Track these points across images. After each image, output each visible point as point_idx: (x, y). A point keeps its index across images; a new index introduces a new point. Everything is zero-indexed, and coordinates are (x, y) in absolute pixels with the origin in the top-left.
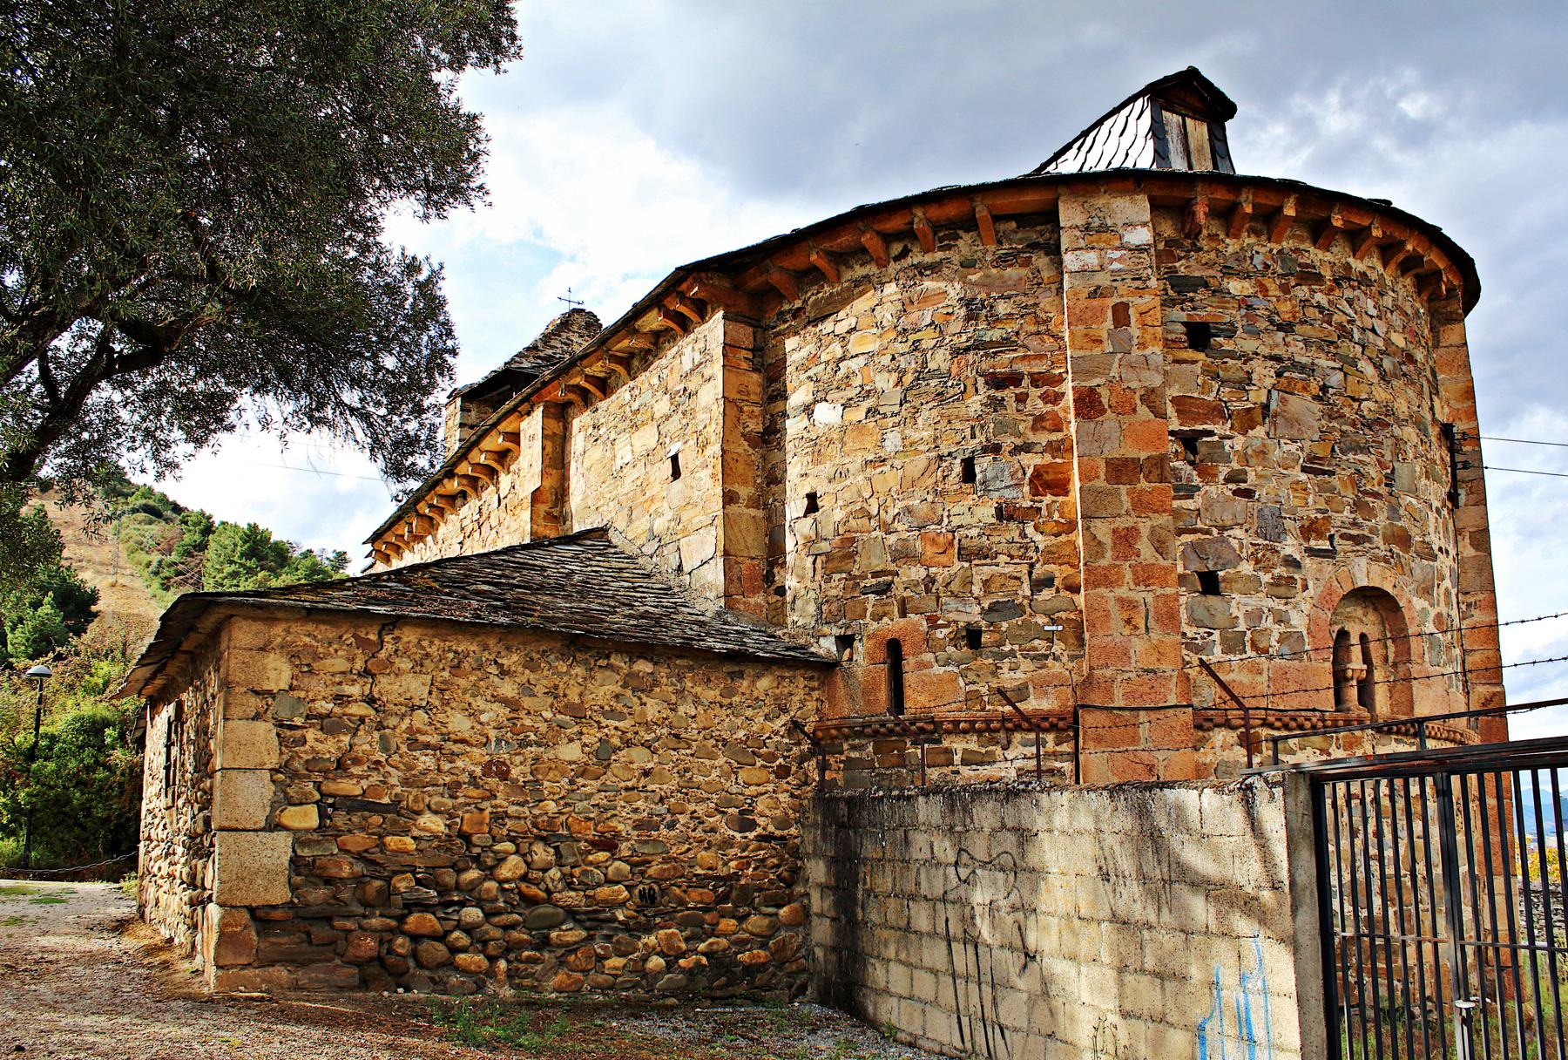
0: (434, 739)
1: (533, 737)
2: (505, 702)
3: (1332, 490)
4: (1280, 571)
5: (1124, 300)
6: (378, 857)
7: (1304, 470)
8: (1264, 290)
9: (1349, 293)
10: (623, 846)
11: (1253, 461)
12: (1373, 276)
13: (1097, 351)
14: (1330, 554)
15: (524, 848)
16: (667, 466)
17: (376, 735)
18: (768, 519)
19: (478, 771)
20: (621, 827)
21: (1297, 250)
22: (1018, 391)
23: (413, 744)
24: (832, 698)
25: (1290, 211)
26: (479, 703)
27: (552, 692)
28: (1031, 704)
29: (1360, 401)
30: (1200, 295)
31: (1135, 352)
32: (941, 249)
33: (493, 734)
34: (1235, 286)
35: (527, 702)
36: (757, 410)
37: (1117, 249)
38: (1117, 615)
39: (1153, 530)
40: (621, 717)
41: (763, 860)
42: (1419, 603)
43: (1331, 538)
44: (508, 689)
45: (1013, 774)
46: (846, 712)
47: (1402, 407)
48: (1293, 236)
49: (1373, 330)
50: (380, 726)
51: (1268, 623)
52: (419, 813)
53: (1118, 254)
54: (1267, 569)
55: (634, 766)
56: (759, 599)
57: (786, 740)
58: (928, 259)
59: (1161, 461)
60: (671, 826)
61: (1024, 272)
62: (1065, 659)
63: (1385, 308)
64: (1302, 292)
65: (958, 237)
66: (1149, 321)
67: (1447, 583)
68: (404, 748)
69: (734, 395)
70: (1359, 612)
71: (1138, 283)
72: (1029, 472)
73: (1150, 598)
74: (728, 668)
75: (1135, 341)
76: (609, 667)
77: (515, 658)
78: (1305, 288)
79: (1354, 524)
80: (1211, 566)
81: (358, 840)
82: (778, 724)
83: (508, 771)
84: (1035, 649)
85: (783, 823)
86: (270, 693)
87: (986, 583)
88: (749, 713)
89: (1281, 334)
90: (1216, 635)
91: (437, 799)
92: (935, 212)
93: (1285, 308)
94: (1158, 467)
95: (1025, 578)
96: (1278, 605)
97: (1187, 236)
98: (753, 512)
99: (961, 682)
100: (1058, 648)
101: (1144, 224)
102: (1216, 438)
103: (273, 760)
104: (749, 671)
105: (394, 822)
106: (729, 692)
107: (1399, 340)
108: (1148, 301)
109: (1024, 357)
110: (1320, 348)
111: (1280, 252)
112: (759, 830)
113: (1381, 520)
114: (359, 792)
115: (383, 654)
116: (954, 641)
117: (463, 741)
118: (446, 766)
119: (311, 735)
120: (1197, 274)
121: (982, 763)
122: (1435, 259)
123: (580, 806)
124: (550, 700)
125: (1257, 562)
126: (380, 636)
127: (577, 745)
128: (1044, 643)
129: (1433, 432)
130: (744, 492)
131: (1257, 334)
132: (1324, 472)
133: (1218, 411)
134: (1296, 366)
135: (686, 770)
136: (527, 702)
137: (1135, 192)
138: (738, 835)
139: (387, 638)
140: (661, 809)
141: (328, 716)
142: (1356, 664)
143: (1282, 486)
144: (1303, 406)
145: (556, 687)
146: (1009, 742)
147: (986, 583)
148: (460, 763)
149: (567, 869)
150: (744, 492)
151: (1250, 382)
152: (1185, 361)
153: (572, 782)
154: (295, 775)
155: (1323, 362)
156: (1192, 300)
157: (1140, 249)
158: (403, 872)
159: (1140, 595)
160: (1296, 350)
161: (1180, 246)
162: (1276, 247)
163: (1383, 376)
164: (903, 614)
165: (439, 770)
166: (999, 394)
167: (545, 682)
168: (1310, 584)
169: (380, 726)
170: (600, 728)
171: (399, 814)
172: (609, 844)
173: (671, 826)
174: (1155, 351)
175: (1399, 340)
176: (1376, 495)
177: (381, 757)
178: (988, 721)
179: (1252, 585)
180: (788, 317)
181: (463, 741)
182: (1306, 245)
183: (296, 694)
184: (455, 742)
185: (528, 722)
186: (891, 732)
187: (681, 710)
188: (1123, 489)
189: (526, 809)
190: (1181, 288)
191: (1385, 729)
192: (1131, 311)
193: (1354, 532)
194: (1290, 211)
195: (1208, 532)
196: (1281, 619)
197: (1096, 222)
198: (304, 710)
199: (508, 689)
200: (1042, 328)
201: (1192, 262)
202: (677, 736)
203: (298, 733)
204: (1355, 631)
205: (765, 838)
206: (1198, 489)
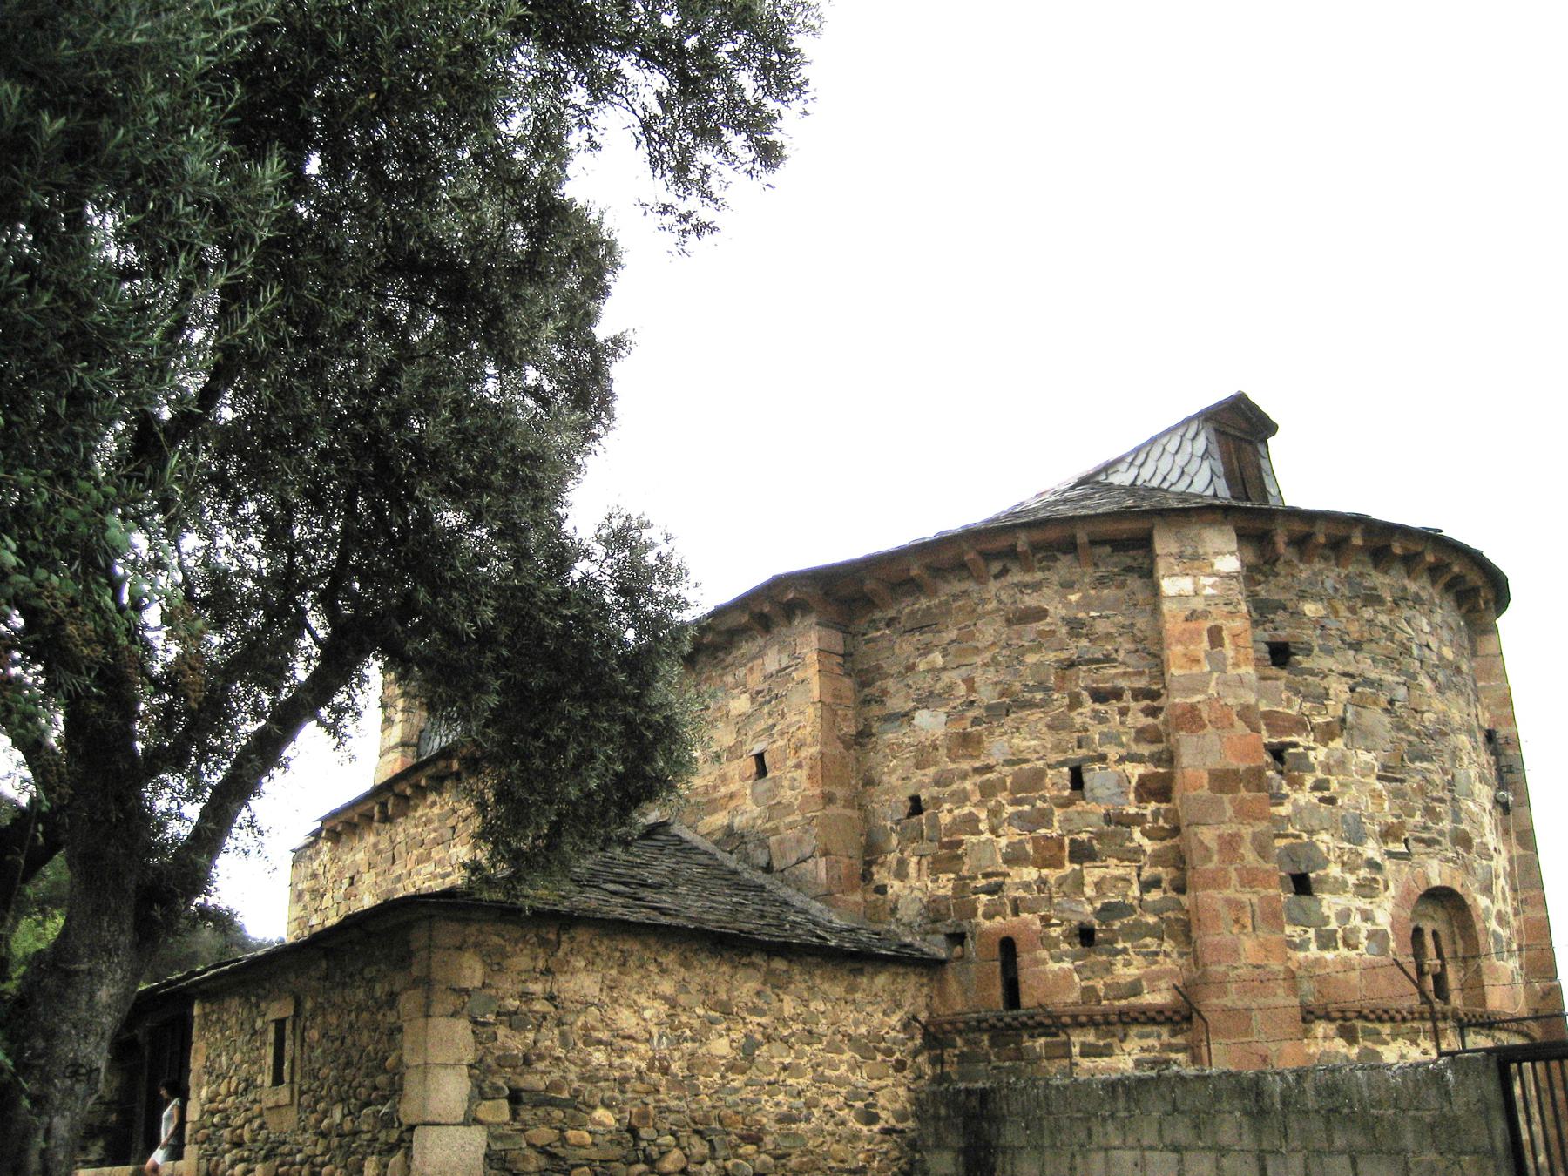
0: (604, 1035)
1: (688, 1033)
2: (665, 999)
3: (1403, 796)
4: (1364, 873)
5: (1218, 622)
6: (561, 1152)
7: (1380, 778)
8: (1336, 613)
9: (1407, 613)
10: (768, 1139)
11: (1334, 770)
12: (1424, 595)
13: (1195, 670)
14: (1405, 856)
15: (684, 1142)
16: (750, 766)
17: (556, 1031)
18: (866, 820)
19: (643, 1066)
20: (765, 1120)
21: (1361, 574)
22: (1120, 705)
23: (589, 1041)
24: (942, 993)
25: (1357, 541)
26: (642, 1001)
27: (705, 990)
28: (1149, 998)
29: (1422, 713)
30: (1280, 616)
31: (1231, 671)
32: (1042, 570)
33: (654, 1030)
34: (1311, 609)
35: (682, 999)
36: (850, 713)
37: (1210, 575)
38: (1227, 915)
39: (1255, 837)
40: (762, 1013)
41: (886, 1153)
42: (1483, 901)
43: (1406, 841)
44: (667, 987)
45: (1131, 1064)
46: (958, 1008)
47: (1456, 716)
48: (1358, 562)
49: (1428, 646)
50: (560, 1023)
51: (1356, 921)
52: (594, 1107)
53: (1210, 580)
54: (1352, 871)
55: (775, 1061)
56: (857, 897)
57: (901, 1036)
58: (1027, 578)
59: (1258, 773)
60: (808, 1120)
61: (1121, 593)
62: (1175, 955)
63: (1430, 627)
64: (1368, 613)
65: (1055, 559)
66: (1241, 642)
67: (1502, 881)
68: (580, 1045)
69: (828, 700)
70: (1430, 911)
71: (1230, 608)
72: (1134, 781)
73: (1255, 899)
74: (849, 965)
75: (1230, 661)
76: (752, 965)
77: (672, 956)
78: (1370, 610)
79: (1426, 828)
80: (1303, 869)
81: (544, 1135)
82: (895, 1020)
83: (668, 1067)
84: (1146, 946)
85: (901, 1117)
86: (466, 991)
87: (1098, 885)
88: (869, 1009)
89: (1352, 652)
90: (1312, 933)
91: (608, 1094)
92: (1038, 536)
93: (1354, 628)
94: (1255, 778)
95: (1135, 880)
96: (1362, 903)
97: (1266, 563)
98: (848, 812)
99: (1076, 978)
100: (1168, 946)
101: (1232, 553)
102: (1301, 750)
103: (470, 1057)
104: (869, 969)
105: (573, 1118)
106: (851, 989)
107: (1448, 653)
108: (1239, 624)
109: (1125, 673)
110: (1386, 665)
111: (1347, 576)
112: (882, 1124)
113: (1446, 825)
114: (543, 1087)
115: (560, 954)
116: (1067, 937)
117: (630, 1037)
118: (617, 1062)
119: (502, 1031)
120: (1276, 597)
121: (1101, 1055)
122: (1475, 578)
123: (730, 1099)
124: (702, 997)
125: (1344, 864)
126: (558, 935)
127: (725, 1041)
128: (1155, 941)
129: (1481, 737)
130: (840, 792)
131: (1329, 652)
132: (1397, 780)
133: (1300, 724)
134: (1369, 682)
135: (819, 1065)
136: (682, 999)
137: (1222, 523)
138: (865, 1129)
139: (564, 938)
140: (799, 1102)
141: (515, 1013)
142: (1432, 960)
143: (1362, 793)
144: (1374, 717)
145: (707, 984)
146: (1126, 1035)
147: (1098, 885)
148: (628, 1059)
149: (720, 1162)
150: (840, 792)
151: (1327, 696)
152: (1270, 678)
153: (723, 1077)
154: (489, 1070)
155: (1390, 678)
156: (1272, 621)
157: (1229, 576)
158: (581, 1166)
159: (1246, 896)
160: (1365, 665)
161: (1260, 571)
162: (1343, 573)
163: (1440, 689)
164: (1016, 913)
165: (610, 1065)
166: (1102, 708)
167: (697, 980)
168: (1391, 884)
169: (560, 1023)
170: (745, 1024)
171: (577, 1107)
172: (755, 1139)
173: (808, 1120)
174: (1248, 671)
175: (1448, 653)
176: (1442, 800)
177: (561, 1052)
178: (1105, 1015)
179: (1339, 887)
180: (882, 625)
181: (630, 1037)
182: (1369, 569)
183: (486, 991)
184: (624, 1038)
185: (684, 1019)
186: (1009, 1026)
187: (813, 1006)
188: (1226, 798)
189: (683, 1103)
190: (1262, 610)
191: (1463, 1026)
192: (1225, 634)
193: (1425, 835)
194: (1357, 541)
195: (1298, 837)
196: (1367, 916)
197: (1189, 551)
198: (495, 1007)
199: (667, 987)
200: (1140, 647)
201: (1272, 586)
202: (810, 1032)
203: (490, 1030)
204: (1428, 927)
205: (886, 1132)
206: (1287, 796)
